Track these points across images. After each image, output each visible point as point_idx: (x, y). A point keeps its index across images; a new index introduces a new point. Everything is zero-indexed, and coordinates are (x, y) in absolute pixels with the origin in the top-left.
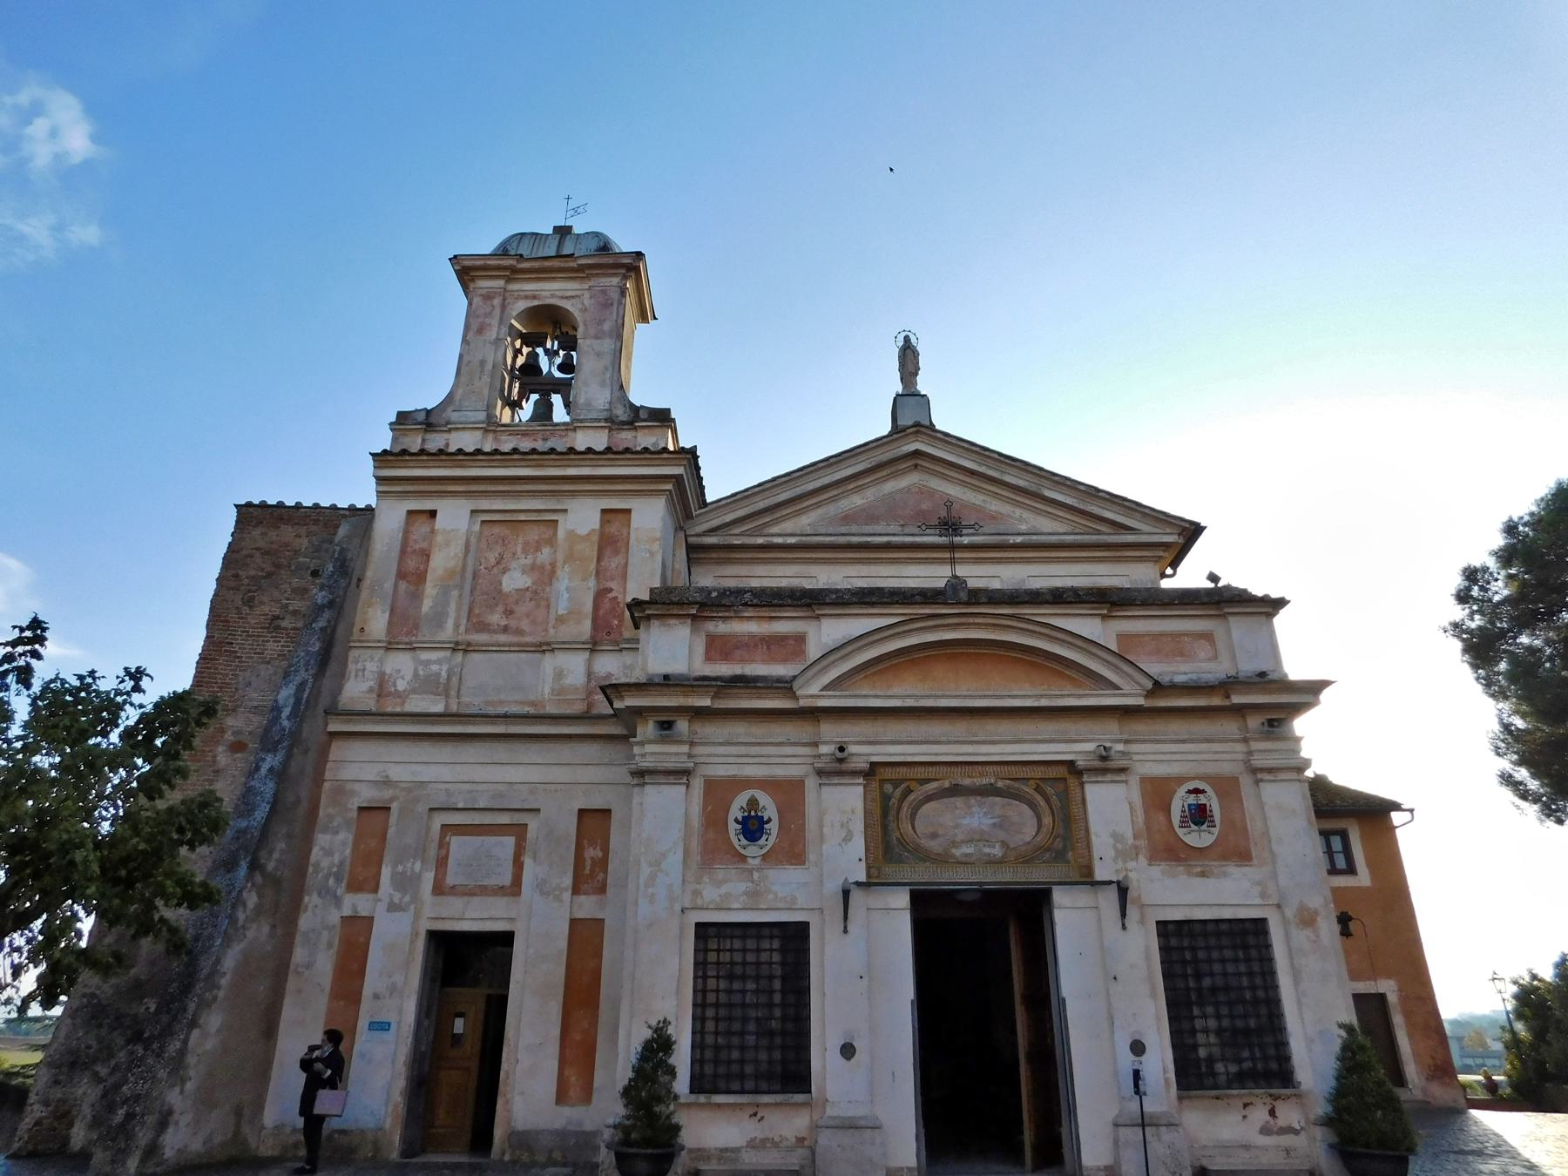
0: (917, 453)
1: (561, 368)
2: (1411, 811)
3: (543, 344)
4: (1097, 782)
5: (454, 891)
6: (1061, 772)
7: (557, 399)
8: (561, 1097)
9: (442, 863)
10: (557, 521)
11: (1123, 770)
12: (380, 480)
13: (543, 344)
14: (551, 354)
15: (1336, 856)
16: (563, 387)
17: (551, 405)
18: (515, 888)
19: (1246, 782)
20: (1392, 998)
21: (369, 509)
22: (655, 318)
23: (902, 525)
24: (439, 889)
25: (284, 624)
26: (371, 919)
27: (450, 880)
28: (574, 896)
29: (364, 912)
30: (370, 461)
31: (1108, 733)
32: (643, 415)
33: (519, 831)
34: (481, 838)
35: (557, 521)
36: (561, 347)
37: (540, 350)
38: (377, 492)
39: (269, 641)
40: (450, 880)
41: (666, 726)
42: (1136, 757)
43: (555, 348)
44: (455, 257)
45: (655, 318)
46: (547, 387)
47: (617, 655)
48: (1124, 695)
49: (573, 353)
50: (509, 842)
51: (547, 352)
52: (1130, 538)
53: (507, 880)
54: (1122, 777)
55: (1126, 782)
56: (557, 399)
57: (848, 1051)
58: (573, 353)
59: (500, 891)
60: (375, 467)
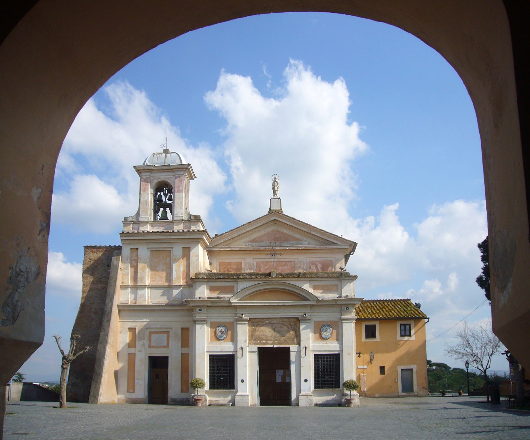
0: (275, 220)
1: (168, 200)
2: (428, 318)
3: (163, 191)
4: (303, 322)
5: (154, 347)
6: (295, 320)
7: (168, 210)
8: (182, 391)
9: (150, 340)
10: (169, 332)
11: (310, 320)
12: (122, 240)
13: (163, 191)
14: (166, 195)
15: (407, 331)
16: (170, 206)
17: (167, 212)
18: (168, 346)
19: (340, 322)
20: (414, 370)
21: (119, 246)
22: (196, 177)
23: (270, 242)
24: (150, 347)
25: (102, 280)
26: (135, 354)
27: (152, 344)
28: (182, 348)
29: (133, 352)
30: (119, 234)
31: (307, 311)
32: (192, 218)
33: (168, 333)
34: (158, 335)
35: (169, 332)
36: (168, 193)
37: (162, 193)
38: (122, 243)
39: (99, 285)
40: (152, 344)
41: (200, 310)
42: (313, 316)
43: (166, 193)
44: (135, 166)
45: (196, 177)
46: (166, 205)
47: (189, 288)
48: (310, 302)
49: (172, 194)
50: (166, 335)
51: (164, 194)
52: (335, 247)
53: (166, 344)
54: (309, 321)
55: (310, 322)
56: (168, 210)
57: (242, 381)
58: (172, 194)
59: (164, 347)
60: (121, 237)
